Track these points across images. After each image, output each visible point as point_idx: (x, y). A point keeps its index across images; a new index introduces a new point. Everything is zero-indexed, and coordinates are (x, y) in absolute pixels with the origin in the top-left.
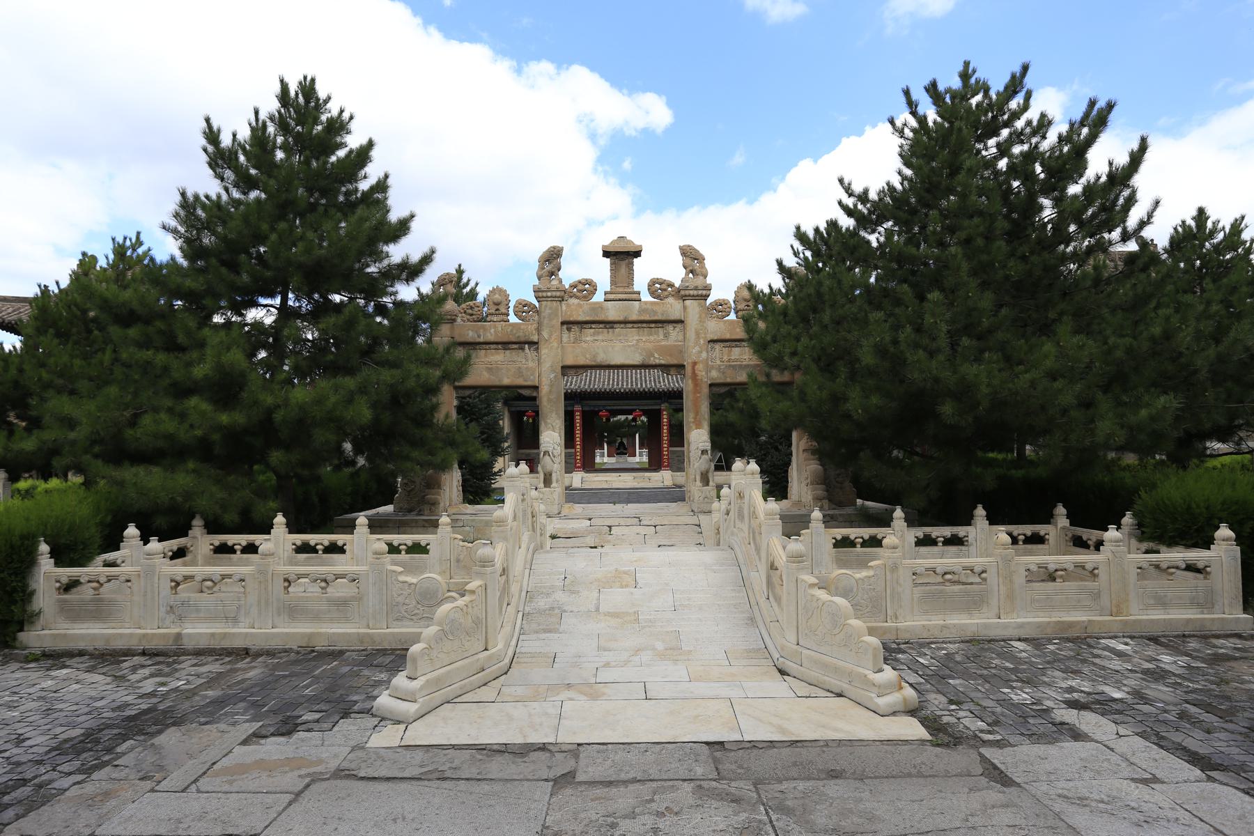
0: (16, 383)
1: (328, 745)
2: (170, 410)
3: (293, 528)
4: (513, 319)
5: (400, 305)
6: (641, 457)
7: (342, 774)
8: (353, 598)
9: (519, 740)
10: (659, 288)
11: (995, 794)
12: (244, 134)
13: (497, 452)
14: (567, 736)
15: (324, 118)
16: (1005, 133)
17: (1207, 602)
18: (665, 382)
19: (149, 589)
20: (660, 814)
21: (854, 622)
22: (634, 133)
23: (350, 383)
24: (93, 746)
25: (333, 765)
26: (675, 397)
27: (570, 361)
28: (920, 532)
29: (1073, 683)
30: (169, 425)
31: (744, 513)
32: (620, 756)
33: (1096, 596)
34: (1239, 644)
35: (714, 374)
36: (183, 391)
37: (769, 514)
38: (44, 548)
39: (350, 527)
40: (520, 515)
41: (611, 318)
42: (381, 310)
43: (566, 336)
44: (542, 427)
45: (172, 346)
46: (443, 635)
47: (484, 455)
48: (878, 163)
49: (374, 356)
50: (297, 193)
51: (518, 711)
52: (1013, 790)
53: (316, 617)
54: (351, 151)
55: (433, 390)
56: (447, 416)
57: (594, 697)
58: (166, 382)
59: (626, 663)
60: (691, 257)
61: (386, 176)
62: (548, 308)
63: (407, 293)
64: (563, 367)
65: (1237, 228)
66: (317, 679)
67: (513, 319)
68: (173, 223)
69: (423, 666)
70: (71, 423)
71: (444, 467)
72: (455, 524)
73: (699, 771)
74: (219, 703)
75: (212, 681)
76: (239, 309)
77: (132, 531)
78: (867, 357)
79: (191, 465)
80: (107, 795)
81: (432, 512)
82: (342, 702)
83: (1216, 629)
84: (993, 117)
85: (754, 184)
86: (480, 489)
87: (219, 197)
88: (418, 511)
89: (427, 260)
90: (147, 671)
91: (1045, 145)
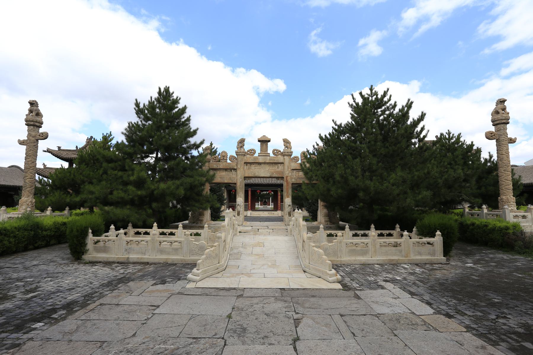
0: (73, 179)
1: (178, 286)
2: (122, 189)
3: (377, 229)
4: (229, 161)
5: (193, 157)
6: (271, 206)
7: (179, 293)
8: (180, 248)
9: (228, 287)
10: (276, 152)
11: (355, 301)
12: (147, 103)
13: (222, 204)
14: (241, 286)
15: (171, 99)
16: (383, 108)
17: (433, 254)
18: (279, 182)
19: (120, 244)
20: (264, 304)
21: (324, 257)
22: (272, 93)
23: (178, 182)
24: (112, 285)
25: (177, 291)
26: (281, 186)
27: (246, 175)
28: (354, 232)
29: (387, 276)
30: (122, 194)
31: (297, 225)
32: (256, 291)
33: (401, 251)
34: (440, 265)
35: (293, 180)
36: (126, 184)
37: (303, 225)
38: (90, 231)
39: (151, 227)
40: (229, 224)
41: (260, 162)
42: (187, 158)
43: (245, 167)
44: (237, 196)
45: (123, 169)
46: (207, 258)
47: (218, 205)
48: (344, 116)
49: (185, 174)
50: (163, 121)
51: (228, 280)
52: (360, 300)
53: (169, 254)
54: (179, 109)
55: (203, 185)
56: (207, 192)
57: (249, 277)
58: (121, 180)
59: (259, 268)
60: (287, 142)
61: (190, 116)
62: (240, 158)
63: (195, 153)
64: (245, 177)
65: (459, 136)
66: (169, 271)
67: (229, 161)
68: (125, 132)
69: (201, 266)
70: (92, 193)
71: (205, 209)
72: (209, 227)
73: (277, 295)
74: (143, 276)
75: (139, 271)
76: (143, 158)
77: (112, 227)
78: (338, 178)
79: (128, 207)
80: (119, 296)
81: (201, 223)
82: (177, 277)
83: (435, 261)
84: (380, 102)
85: (313, 111)
86: (216, 216)
87: (138, 122)
88: (196, 223)
89: (202, 143)
90: (120, 268)
91: (395, 112)
